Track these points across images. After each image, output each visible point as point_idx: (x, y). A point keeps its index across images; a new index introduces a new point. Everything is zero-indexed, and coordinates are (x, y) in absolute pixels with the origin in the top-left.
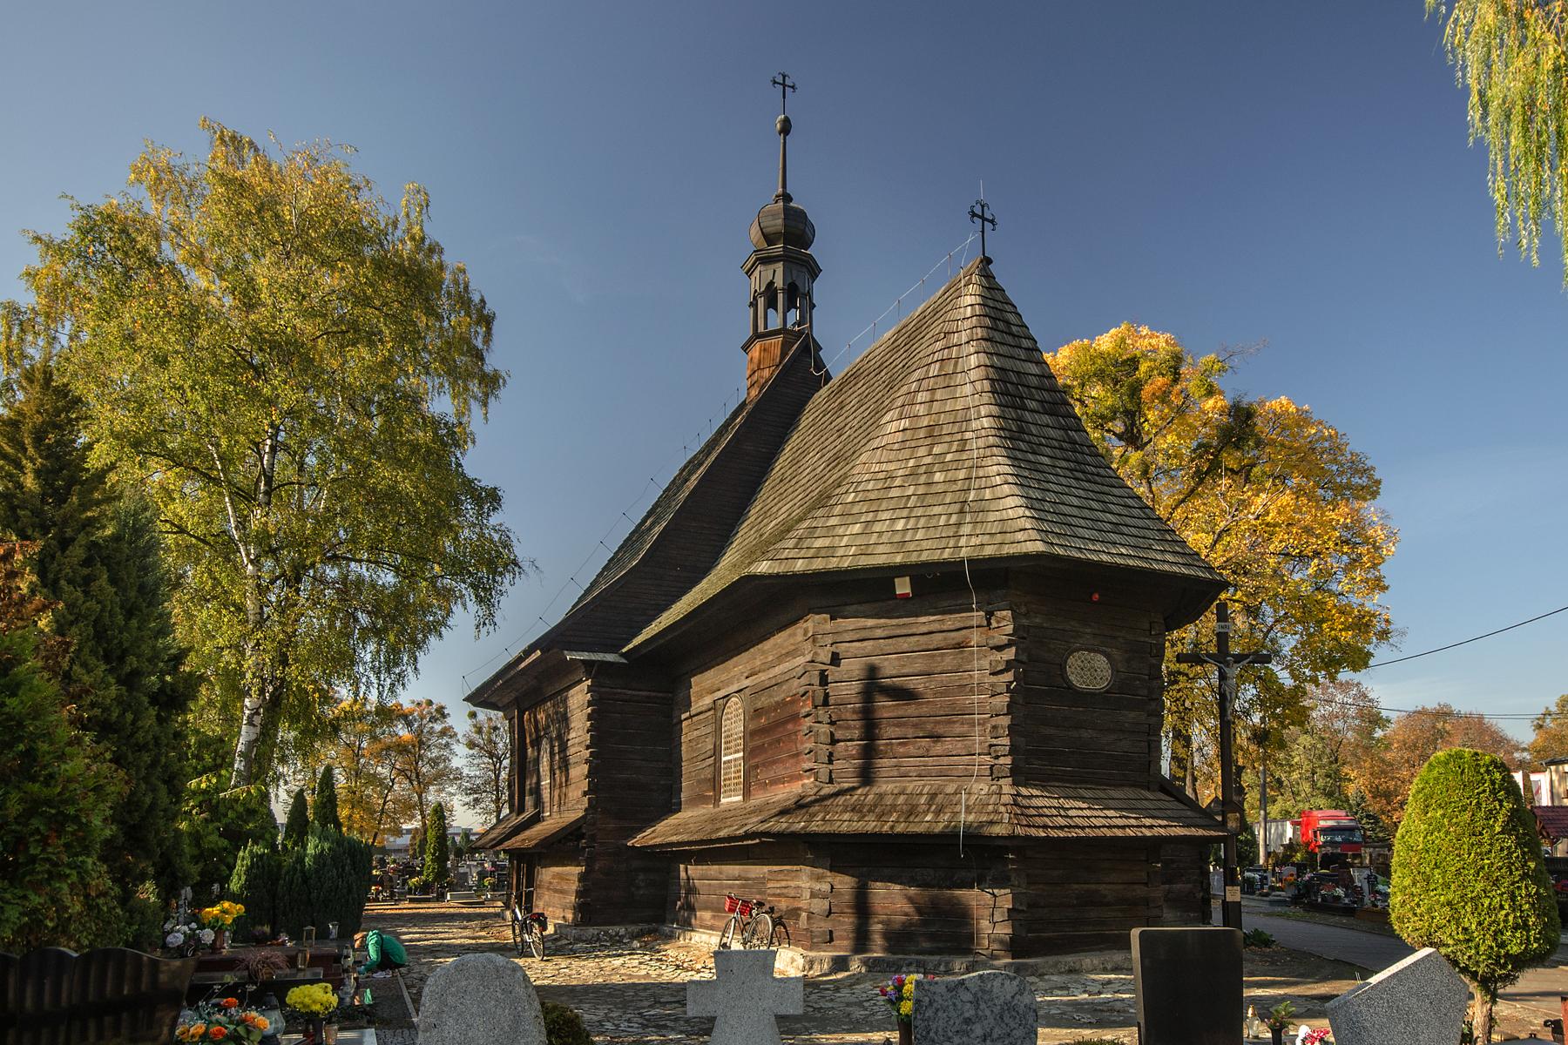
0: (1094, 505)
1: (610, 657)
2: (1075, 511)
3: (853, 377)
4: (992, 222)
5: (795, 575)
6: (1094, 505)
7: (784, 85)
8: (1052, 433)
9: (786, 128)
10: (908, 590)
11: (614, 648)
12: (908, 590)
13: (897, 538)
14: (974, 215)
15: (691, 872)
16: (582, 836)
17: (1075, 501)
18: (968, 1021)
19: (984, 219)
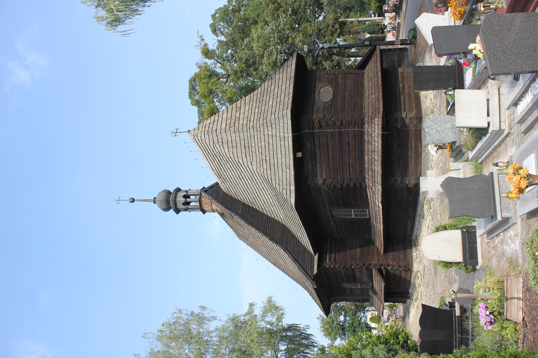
0: (272, 94)
1: (316, 258)
2: (275, 100)
3: (219, 176)
4: (177, 130)
5: (296, 189)
6: (272, 94)
7: (119, 200)
8: (247, 108)
9: (133, 200)
10: (300, 153)
11: (313, 259)
12: (300, 153)
13: (373, 143)
14: (175, 135)
15: (385, 65)
16: (380, 268)
17: (271, 100)
18: (437, 131)
19: (177, 132)
